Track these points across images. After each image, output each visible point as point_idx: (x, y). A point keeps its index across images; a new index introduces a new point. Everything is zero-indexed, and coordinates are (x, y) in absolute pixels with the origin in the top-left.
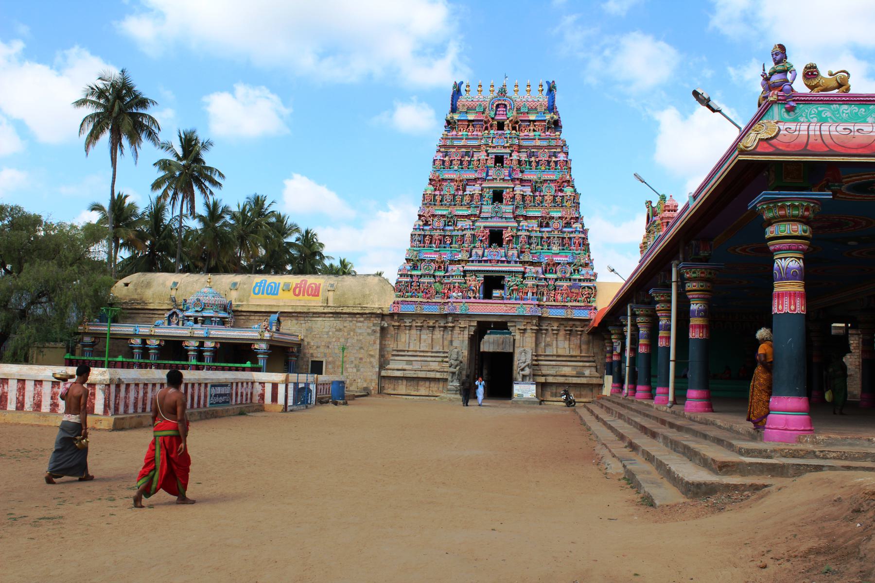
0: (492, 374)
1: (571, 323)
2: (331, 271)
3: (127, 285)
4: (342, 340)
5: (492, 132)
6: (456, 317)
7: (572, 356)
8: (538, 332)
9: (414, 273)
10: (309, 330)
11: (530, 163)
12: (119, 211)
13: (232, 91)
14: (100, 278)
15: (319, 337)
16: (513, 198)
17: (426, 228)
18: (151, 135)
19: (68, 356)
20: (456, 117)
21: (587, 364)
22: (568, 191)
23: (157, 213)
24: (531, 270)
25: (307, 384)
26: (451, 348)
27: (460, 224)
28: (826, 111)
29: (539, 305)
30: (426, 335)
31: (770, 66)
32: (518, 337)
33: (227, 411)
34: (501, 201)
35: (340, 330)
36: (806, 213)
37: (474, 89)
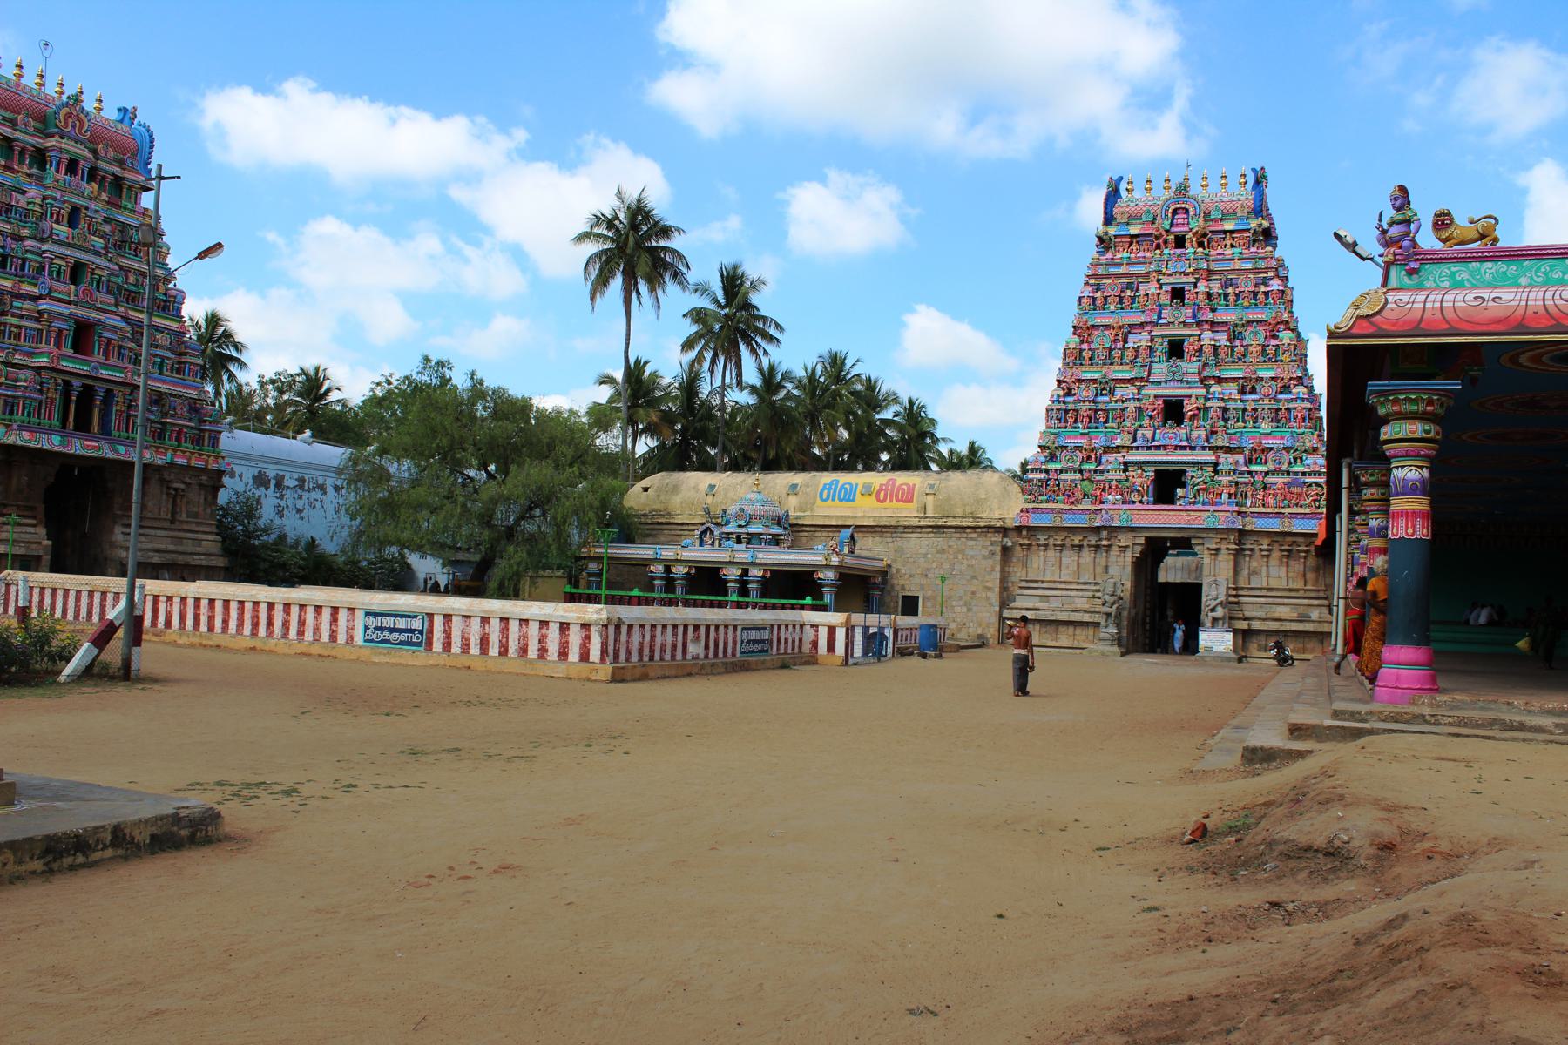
0: (1161, 615)
1: (1290, 539)
2: (955, 464)
3: (646, 490)
4: (946, 566)
5: (1166, 251)
6: (1113, 531)
7: (1291, 590)
8: (1239, 553)
9: (1051, 466)
10: (899, 551)
11: (1226, 296)
12: (637, 385)
13: (823, 180)
14: (608, 482)
15: (911, 563)
16: (1200, 350)
17: (1068, 399)
18: (677, 275)
19: (568, 589)
20: (1112, 231)
21: (1316, 602)
22: (1286, 337)
23: (690, 385)
24: (1226, 459)
25: (881, 629)
26: (1106, 577)
27: (1119, 393)
28: (1462, 271)
29: (1239, 513)
30: (1069, 558)
31: (1390, 213)
32: (1207, 560)
33: (763, 662)
34: (1181, 356)
35: (943, 551)
36: (1429, 409)
37: (1139, 186)
